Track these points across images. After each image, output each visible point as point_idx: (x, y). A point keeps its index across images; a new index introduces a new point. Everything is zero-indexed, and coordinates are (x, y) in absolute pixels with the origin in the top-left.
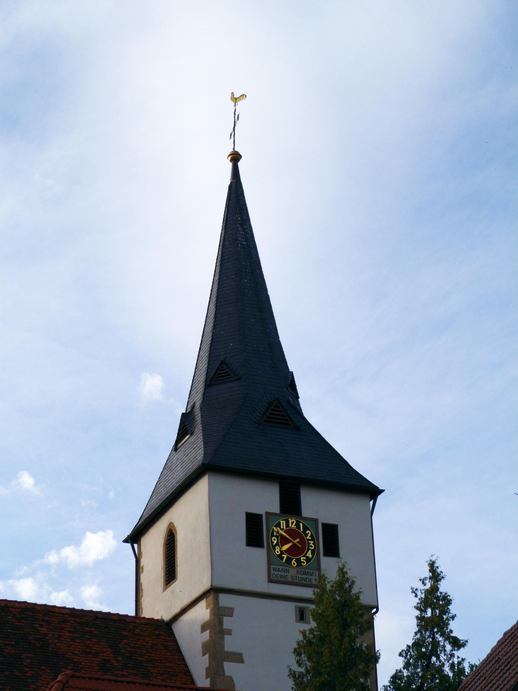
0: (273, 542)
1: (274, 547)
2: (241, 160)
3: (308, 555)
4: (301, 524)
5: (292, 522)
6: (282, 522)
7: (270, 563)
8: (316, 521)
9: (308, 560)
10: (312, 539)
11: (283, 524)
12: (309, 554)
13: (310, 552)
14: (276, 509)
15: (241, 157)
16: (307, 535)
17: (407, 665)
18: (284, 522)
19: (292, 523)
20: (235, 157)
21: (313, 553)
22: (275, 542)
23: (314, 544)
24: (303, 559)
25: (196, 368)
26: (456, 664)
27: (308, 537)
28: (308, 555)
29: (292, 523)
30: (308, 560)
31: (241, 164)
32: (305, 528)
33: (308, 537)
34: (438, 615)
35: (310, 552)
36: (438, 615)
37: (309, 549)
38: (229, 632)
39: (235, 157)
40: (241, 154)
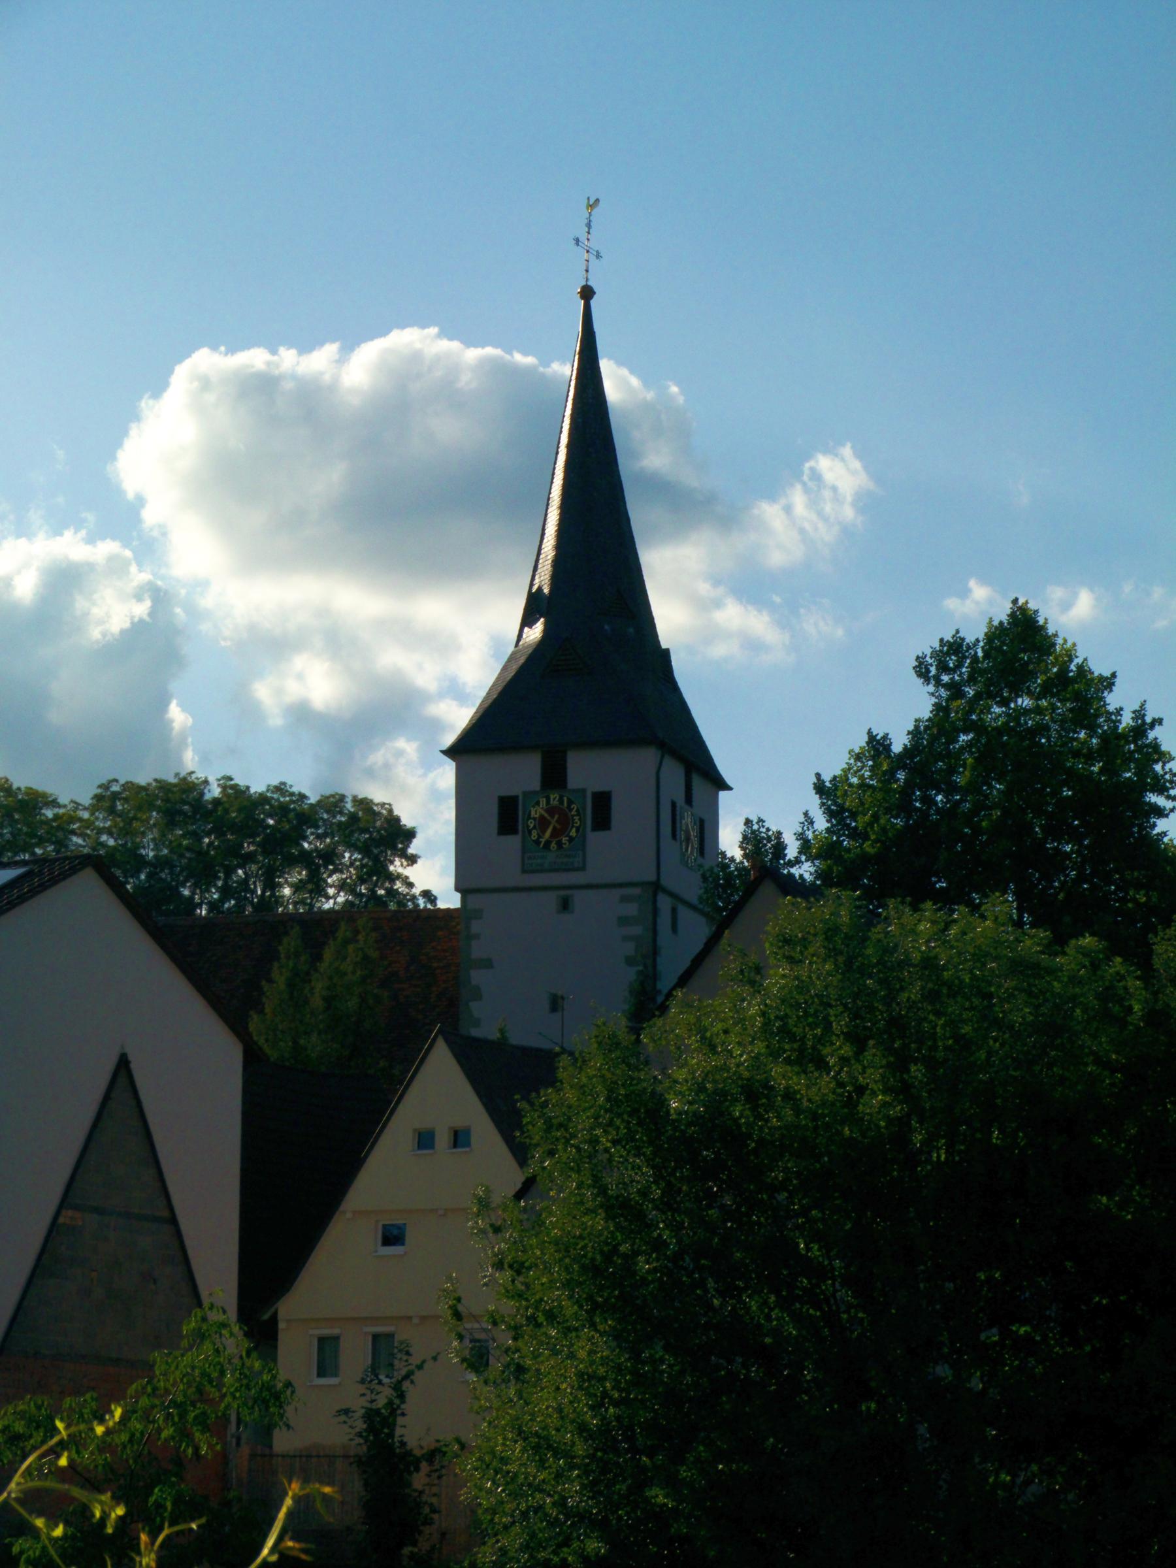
0: (528, 826)
1: (530, 832)
2: (595, 297)
3: (571, 834)
4: (565, 799)
5: (554, 797)
6: (541, 800)
7: (524, 850)
8: (584, 791)
9: (571, 839)
10: (578, 814)
11: (543, 802)
12: (573, 833)
13: (574, 830)
14: (536, 785)
15: (594, 293)
16: (571, 810)
17: (706, 892)
18: (544, 799)
19: (554, 799)
20: (587, 293)
21: (578, 831)
22: (532, 826)
23: (580, 819)
24: (564, 840)
25: (13, 1320)
26: (280, 1381)
27: (573, 813)
28: (571, 834)
29: (554, 799)
30: (571, 839)
31: (593, 303)
32: (570, 802)
33: (573, 813)
34: (110, 1530)
35: (574, 830)
36: (110, 1530)
37: (573, 826)
38: (477, 936)
39: (587, 293)
40: (595, 290)
